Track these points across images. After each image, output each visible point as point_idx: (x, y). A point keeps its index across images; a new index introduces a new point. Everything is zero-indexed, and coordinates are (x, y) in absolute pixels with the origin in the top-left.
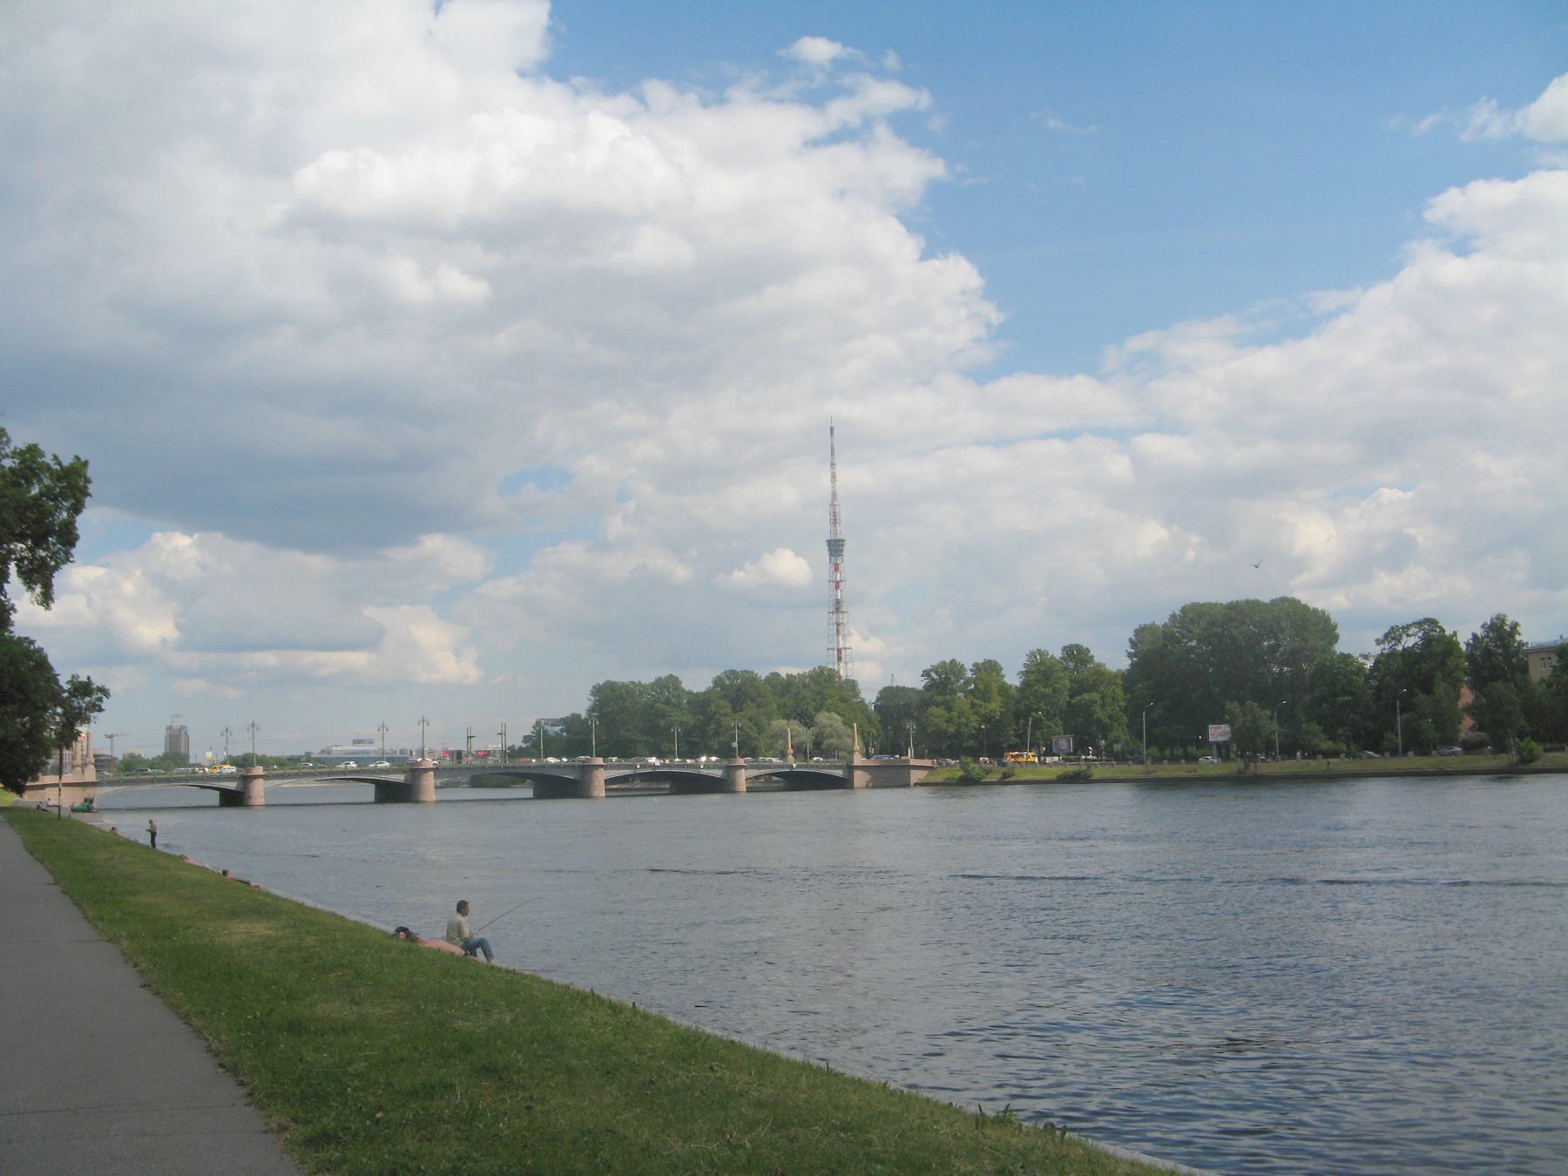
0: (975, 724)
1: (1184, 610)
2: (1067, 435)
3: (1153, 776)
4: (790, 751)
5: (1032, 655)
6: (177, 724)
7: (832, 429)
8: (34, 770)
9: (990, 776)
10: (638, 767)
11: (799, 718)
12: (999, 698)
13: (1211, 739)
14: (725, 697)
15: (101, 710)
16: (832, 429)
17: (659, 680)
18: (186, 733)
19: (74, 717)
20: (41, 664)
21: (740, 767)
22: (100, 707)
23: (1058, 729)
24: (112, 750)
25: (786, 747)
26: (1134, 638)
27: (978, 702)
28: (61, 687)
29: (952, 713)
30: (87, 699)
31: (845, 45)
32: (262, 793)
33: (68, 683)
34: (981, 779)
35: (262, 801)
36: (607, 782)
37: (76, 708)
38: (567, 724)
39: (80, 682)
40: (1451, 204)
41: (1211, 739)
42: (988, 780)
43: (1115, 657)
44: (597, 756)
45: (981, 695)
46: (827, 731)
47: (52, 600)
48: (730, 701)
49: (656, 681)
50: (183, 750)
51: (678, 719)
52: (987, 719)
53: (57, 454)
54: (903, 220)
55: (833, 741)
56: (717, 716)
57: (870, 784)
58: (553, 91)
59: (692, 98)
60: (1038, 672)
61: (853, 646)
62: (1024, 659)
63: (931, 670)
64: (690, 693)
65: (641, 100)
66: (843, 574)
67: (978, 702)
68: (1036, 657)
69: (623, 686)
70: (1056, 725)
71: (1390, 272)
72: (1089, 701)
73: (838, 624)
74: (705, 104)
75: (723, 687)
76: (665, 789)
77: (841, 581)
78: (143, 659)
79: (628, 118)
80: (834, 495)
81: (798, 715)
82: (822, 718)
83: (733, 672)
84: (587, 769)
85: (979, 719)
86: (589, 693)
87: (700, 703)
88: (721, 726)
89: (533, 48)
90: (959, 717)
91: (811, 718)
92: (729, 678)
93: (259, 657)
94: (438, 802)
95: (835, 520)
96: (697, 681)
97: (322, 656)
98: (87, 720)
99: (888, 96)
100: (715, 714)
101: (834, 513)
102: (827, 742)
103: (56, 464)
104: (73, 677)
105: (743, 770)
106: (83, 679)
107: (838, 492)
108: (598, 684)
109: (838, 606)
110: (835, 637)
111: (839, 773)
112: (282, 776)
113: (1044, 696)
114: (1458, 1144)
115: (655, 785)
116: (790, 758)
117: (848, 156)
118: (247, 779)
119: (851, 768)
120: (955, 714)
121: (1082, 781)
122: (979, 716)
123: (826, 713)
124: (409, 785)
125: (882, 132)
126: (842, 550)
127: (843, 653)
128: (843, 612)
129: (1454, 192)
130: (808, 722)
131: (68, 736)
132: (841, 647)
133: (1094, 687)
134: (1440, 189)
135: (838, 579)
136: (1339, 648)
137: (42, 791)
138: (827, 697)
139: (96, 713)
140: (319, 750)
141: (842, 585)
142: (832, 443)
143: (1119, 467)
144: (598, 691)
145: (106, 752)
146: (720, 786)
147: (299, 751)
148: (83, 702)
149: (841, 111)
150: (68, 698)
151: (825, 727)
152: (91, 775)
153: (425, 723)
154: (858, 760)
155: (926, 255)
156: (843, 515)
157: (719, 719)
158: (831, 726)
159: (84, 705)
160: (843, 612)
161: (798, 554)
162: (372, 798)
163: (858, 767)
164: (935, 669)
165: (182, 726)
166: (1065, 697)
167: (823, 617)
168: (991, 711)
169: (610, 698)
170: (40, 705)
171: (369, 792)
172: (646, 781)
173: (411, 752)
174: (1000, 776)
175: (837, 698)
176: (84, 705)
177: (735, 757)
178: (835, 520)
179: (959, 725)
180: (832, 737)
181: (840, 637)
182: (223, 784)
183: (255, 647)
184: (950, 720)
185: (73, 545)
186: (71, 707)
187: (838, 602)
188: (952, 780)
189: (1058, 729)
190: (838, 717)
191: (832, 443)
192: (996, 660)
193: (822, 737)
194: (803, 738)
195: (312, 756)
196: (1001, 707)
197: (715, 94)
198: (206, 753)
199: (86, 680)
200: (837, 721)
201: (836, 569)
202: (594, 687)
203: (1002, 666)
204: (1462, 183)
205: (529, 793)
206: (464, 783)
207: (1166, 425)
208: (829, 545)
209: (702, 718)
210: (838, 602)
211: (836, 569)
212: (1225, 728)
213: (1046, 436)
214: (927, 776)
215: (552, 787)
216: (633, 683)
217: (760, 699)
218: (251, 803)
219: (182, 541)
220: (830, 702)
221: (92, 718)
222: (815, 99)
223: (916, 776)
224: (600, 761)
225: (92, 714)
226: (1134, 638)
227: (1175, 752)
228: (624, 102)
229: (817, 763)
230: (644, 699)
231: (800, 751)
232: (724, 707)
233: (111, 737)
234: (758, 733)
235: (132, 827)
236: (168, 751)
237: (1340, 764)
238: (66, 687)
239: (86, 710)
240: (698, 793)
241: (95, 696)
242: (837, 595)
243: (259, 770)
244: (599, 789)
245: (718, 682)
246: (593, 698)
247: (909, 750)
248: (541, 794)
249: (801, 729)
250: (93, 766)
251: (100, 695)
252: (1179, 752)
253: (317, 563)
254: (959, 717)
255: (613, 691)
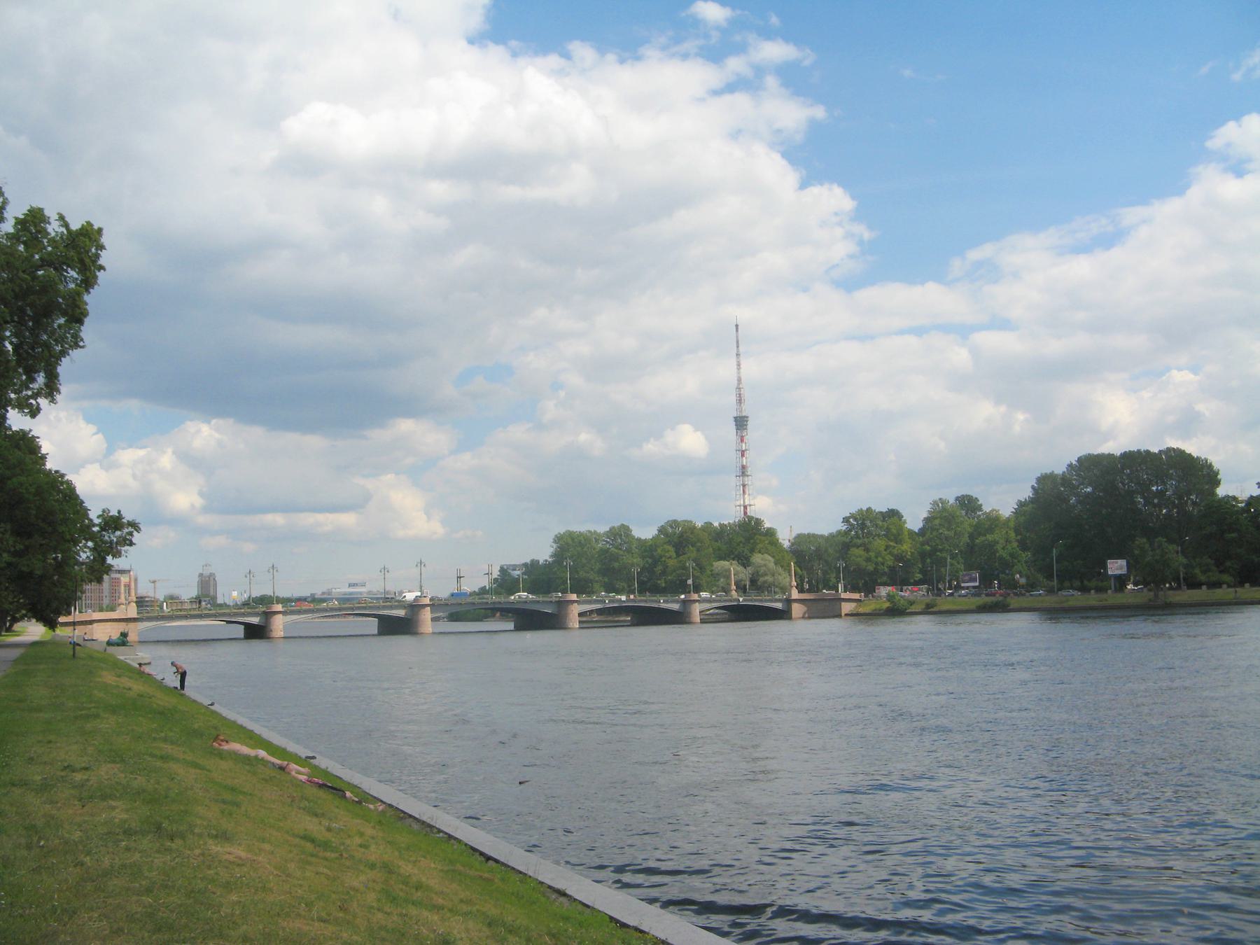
0: (890, 563)
1: (1079, 460)
2: (919, 331)
3: (1065, 605)
4: (734, 587)
5: (935, 503)
6: (206, 573)
7: (737, 326)
8: (66, 605)
9: (913, 607)
10: (607, 602)
11: (736, 559)
12: (910, 541)
13: (1110, 572)
14: (669, 543)
15: (131, 544)
16: (737, 326)
17: (612, 529)
18: (214, 579)
19: (104, 550)
20: (70, 496)
21: (695, 601)
22: (131, 541)
23: (959, 566)
24: (155, 593)
25: (729, 584)
26: (1036, 485)
27: (892, 544)
28: (91, 520)
29: (870, 553)
30: (118, 533)
31: (733, 8)
32: (281, 627)
33: (98, 517)
34: (906, 609)
35: (282, 634)
36: (580, 615)
37: (106, 542)
38: (528, 567)
39: (112, 517)
40: (1229, 133)
41: (1110, 572)
42: (913, 610)
43: (914, 520)
44: (571, 593)
45: (892, 538)
46: (762, 570)
47: (58, 391)
48: (673, 546)
49: (610, 529)
50: (212, 593)
51: (630, 562)
52: (899, 558)
53: (64, 214)
54: (785, 155)
55: (769, 579)
56: (663, 559)
57: (807, 615)
58: (496, 53)
59: (611, 57)
60: (941, 518)
61: (756, 503)
62: (928, 507)
63: (849, 517)
64: (639, 540)
65: (567, 56)
66: (747, 445)
67: (892, 544)
68: (938, 506)
69: (581, 534)
70: (958, 563)
71: (1180, 191)
72: (992, 541)
73: (744, 486)
74: (622, 61)
75: (666, 535)
76: (625, 621)
77: (746, 450)
78: (177, 521)
79: (559, 73)
80: (739, 380)
81: (736, 556)
82: (757, 559)
83: (675, 521)
84: (563, 605)
85: (892, 558)
86: (552, 541)
87: (648, 549)
88: (667, 567)
89: (476, 21)
90: (876, 557)
91: (748, 559)
92: (672, 527)
93: (270, 518)
94: (434, 633)
95: (740, 401)
96: (645, 532)
97: (320, 517)
98: (117, 554)
99: (775, 51)
100: (661, 557)
101: (740, 394)
102: (762, 579)
103: (62, 226)
104: (104, 511)
105: (697, 604)
106: (114, 513)
107: (742, 378)
108: (560, 534)
109: (743, 471)
110: (742, 496)
111: (779, 605)
112: (299, 612)
113: (947, 539)
114: (1210, 895)
115: (610, 618)
116: (734, 593)
117: (741, 101)
118: (268, 615)
119: (789, 601)
120: (872, 554)
121: (1000, 610)
122: (892, 556)
123: (760, 555)
124: (555, 615)
125: (771, 81)
126: (746, 425)
127: (748, 509)
128: (748, 476)
129: (1231, 125)
130: (745, 561)
131: (98, 570)
132: (746, 504)
133: (990, 530)
134: (1220, 122)
135: (744, 449)
136: (1221, 491)
137: (90, 626)
138: (758, 541)
139: (127, 548)
140: (320, 593)
141: (747, 454)
142: (737, 337)
143: (960, 356)
144: (558, 539)
145: (151, 594)
146: (678, 618)
147: (318, 591)
148: (115, 536)
149: (735, 65)
150: (98, 532)
151: (760, 567)
152: (132, 612)
153: (422, 565)
154: (795, 594)
155: (804, 185)
156: (746, 394)
157: (665, 561)
158: (765, 565)
159: (115, 540)
160: (748, 476)
161: (697, 429)
162: (376, 632)
163: (796, 601)
164: (852, 516)
165: (211, 573)
166: (966, 539)
167: (733, 480)
168: (903, 552)
169: (569, 545)
170: (68, 537)
171: (372, 625)
172: (601, 615)
173: (395, 594)
174: (924, 607)
175: (766, 542)
176: (115, 540)
177: (689, 592)
178: (740, 400)
179: (877, 564)
180: (766, 575)
181: (746, 496)
182: (245, 619)
183: (273, 509)
184: (868, 560)
185: (80, 321)
186: (101, 540)
187: (743, 467)
188: (880, 610)
189: (959, 566)
190: (770, 558)
191: (737, 337)
192: (899, 509)
193: (758, 575)
194: (741, 576)
195: (316, 597)
196: (911, 548)
197: (629, 50)
198: (231, 593)
199: (117, 515)
200: (770, 561)
201: (742, 441)
202: (556, 536)
203: (903, 514)
204: (1237, 116)
205: (511, 626)
206: (443, 618)
207: (1002, 324)
208: (735, 421)
209: (650, 561)
210: (743, 467)
211: (742, 441)
212: (1123, 563)
213: (901, 332)
214: (856, 607)
215: (529, 620)
216: (590, 532)
217: (699, 544)
218: (422, 631)
219: (205, 429)
220: (761, 546)
221: (123, 552)
222: (714, 55)
223: (847, 608)
224: (574, 597)
225: (123, 548)
226: (1036, 485)
227: (1079, 584)
228: (554, 60)
229: (755, 600)
230: (600, 545)
231: (741, 588)
232: (668, 551)
233: (154, 582)
234: (701, 573)
235: (162, 669)
236: (200, 593)
237: (1223, 593)
238: (97, 521)
239: (117, 543)
240: (542, 629)
241: (126, 530)
242: (742, 462)
243: (279, 607)
244: (574, 621)
245: (662, 530)
246: (555, 546)
247: (840, 585)
248: (520, 628)
249: (740, 568)
250: (135, 604)
251: (130, 529)
252: (1077, 583)
253: (314, 442)
254: (876, 557)
255: (573, 540)
